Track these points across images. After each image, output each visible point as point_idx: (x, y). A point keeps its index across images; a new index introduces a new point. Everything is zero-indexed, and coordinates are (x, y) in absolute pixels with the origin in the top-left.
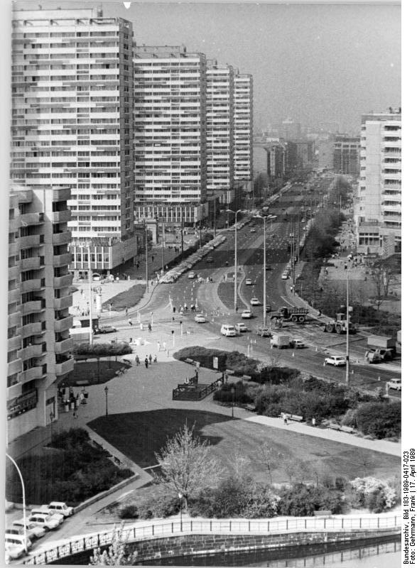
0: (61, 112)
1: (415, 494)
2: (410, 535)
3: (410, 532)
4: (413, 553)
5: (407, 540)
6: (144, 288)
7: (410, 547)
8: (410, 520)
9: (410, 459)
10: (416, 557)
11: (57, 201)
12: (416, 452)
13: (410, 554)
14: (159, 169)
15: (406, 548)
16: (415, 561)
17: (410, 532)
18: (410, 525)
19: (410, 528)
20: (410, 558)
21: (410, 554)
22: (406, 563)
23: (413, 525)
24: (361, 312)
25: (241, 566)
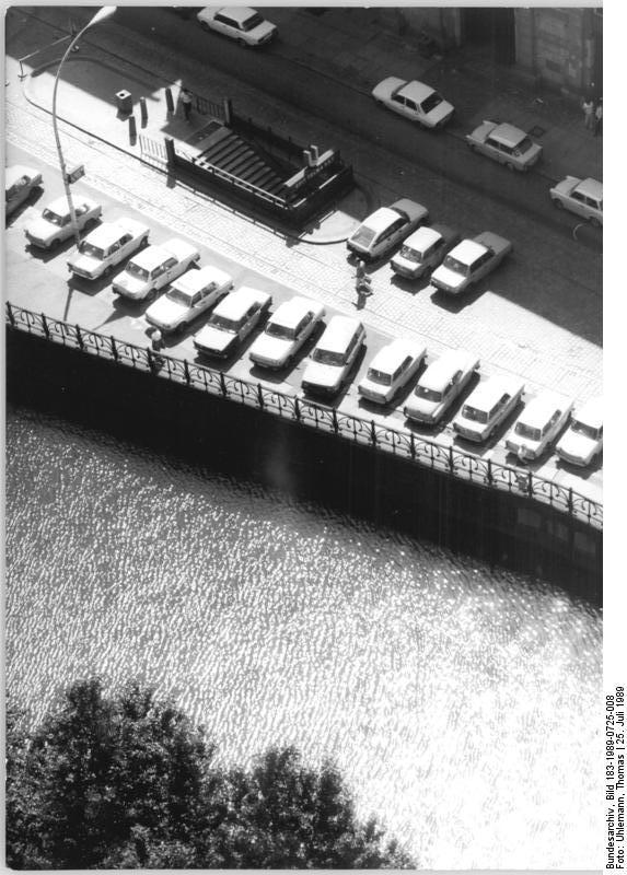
0: (210, 133)
1: (625, 752)
2: (616, 826)
3: (616, 819)
4: (621, 852)
6: (353, 238)
7: (616, 844)
8: (616, 801)
9: (616, 703)
10: (625, 858)
11: (523, 47)
12: (625, 692)
13: (616, 854)
14: (245, 184)
16: (625, 865)
17: (616, 819)
18: (616, 809)
19: (616, 814)
20: (616, 860)
21: (616, 854)
22: (610, 866)
23: (621, 809)
24: (565, 711)
25: (470, 14)
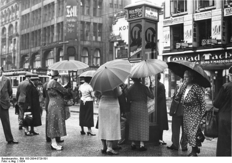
4: (6, 161)
13: (6, 160)
15: (8, 159)
20: (4, 160)
21: (6, 160)
22: (2, 158)
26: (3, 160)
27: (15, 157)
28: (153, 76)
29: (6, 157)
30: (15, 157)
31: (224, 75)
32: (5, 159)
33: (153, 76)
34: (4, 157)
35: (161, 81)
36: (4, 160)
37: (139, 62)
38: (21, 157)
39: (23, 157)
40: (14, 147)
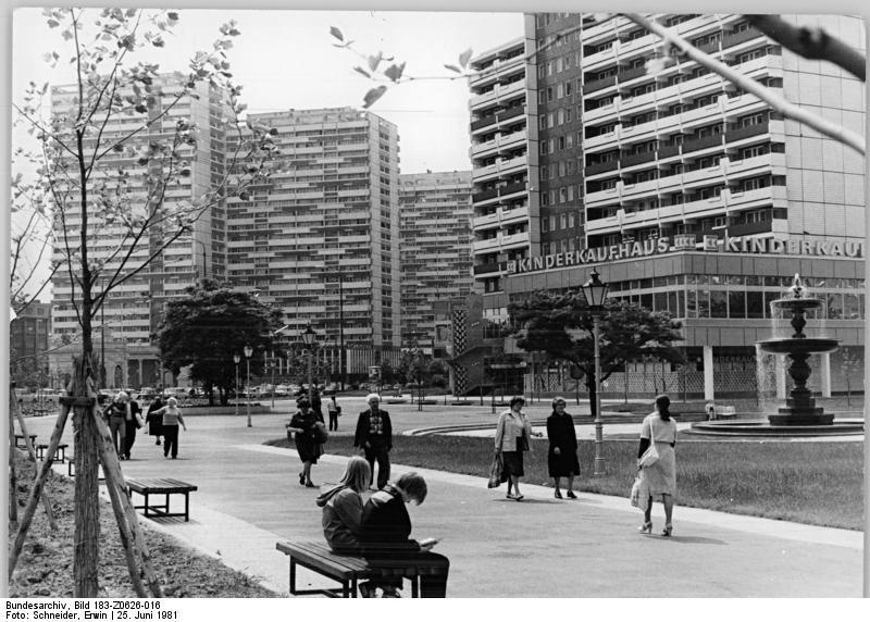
4: (23, 616)
5: (42, 606)
8: (73, 611)
13: (21, 611)
15: (30, 606)
20: (15, 611)
21: (21, 611)
22: (8, 605)
26: (11, 610)
27: (57, 600)
28: (185, 371)
29: (22, 601)
30: (57, 600)
31: (251, 351)
32: (17, 606)
33: (185, 371)
34: (14, 601)
35: (765, 423)
36: (15, 611)
37: (469, 403)
38: (79, 600)
39: (86, 600)
40: (659, 366)
